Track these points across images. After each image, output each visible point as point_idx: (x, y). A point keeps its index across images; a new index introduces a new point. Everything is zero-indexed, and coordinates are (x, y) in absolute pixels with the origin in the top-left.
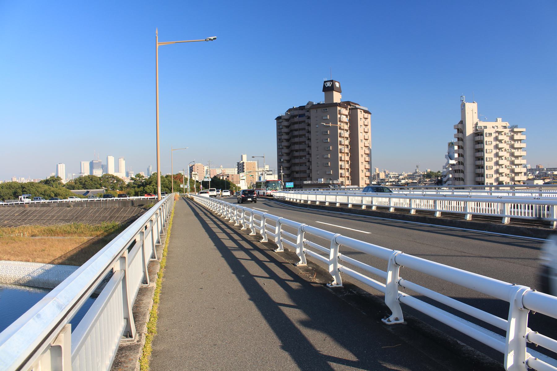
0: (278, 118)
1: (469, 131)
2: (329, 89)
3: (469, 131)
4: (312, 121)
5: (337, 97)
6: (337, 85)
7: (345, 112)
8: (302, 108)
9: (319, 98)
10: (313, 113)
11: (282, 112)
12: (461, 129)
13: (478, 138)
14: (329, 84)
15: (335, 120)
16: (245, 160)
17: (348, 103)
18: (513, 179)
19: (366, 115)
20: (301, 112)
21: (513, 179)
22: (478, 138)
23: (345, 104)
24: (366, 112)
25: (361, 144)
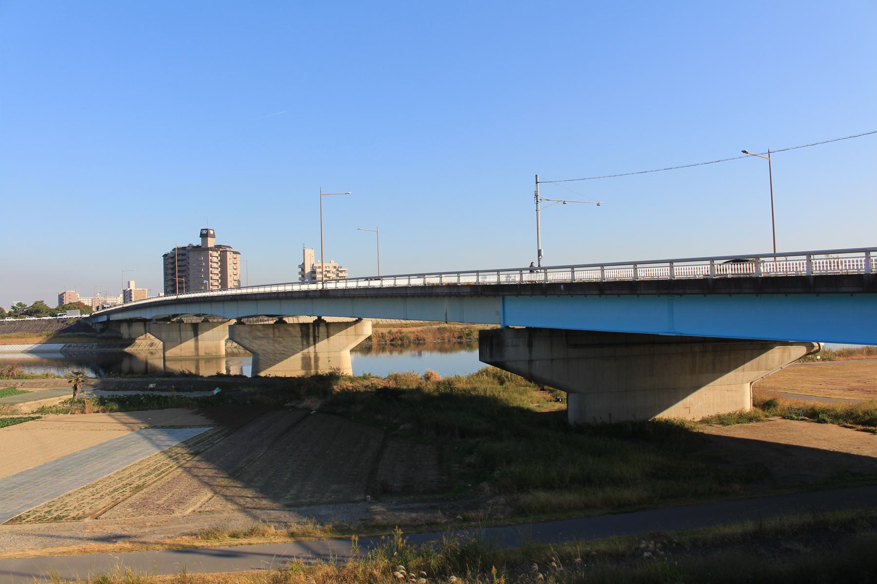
0: (165, 256)
1: (308, 270)
2: (205, 235)
3: (308, 270)
4: (191, 260)
5: (211, 243)
6: (212, 232)
7: (215, 254)
8: (184, 248)
9: (198, 242)
10: (191, 254)
11: (169, 250)
12: (303, 267)
13: (313, 275)
14: (205, 232)
15: (207, 261)
16: (133, 287)
17: (219, 247)
18: (337, 275)
19: (235, 256)
20: (183, 252)
21: (337, 275)
22: (313, 275)
23: (217, 247)
24: (235, 253)
25: (229, 279)
